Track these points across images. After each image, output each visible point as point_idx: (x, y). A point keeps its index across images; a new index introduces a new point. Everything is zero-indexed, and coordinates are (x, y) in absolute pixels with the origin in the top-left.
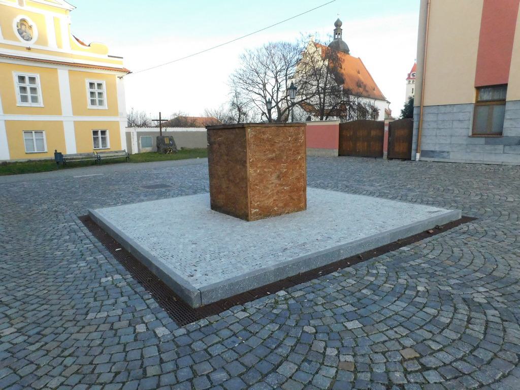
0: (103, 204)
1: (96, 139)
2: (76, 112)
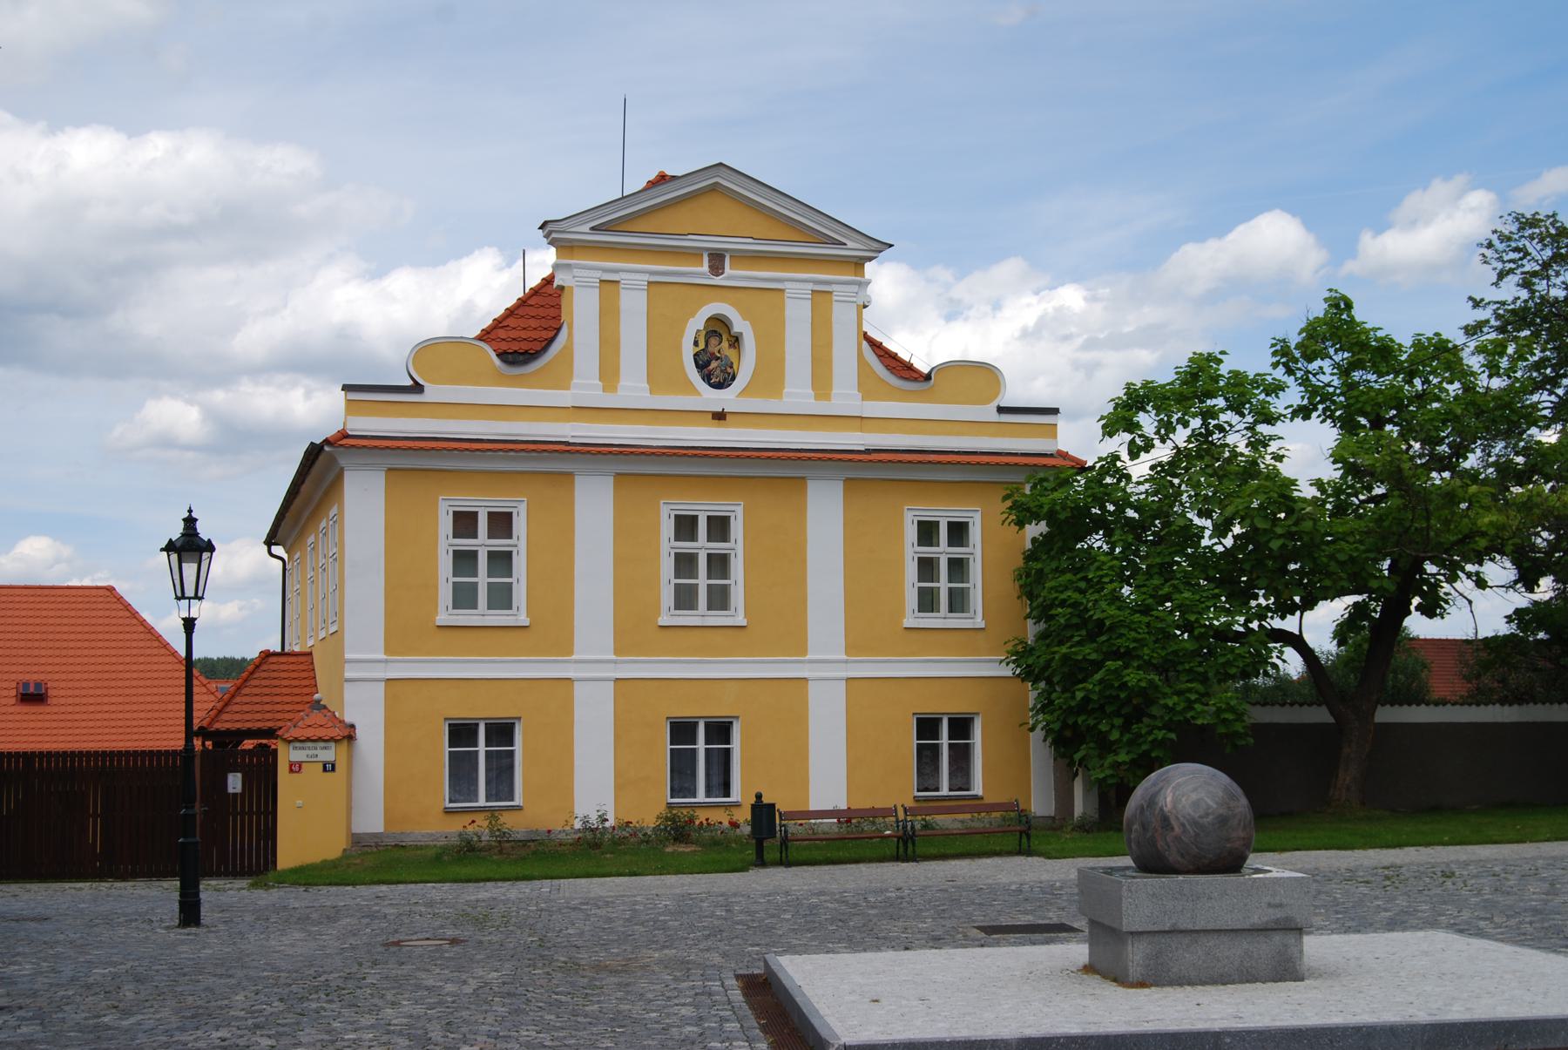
0: (791, 950)
1: (927, 758)
2: (857, 644)
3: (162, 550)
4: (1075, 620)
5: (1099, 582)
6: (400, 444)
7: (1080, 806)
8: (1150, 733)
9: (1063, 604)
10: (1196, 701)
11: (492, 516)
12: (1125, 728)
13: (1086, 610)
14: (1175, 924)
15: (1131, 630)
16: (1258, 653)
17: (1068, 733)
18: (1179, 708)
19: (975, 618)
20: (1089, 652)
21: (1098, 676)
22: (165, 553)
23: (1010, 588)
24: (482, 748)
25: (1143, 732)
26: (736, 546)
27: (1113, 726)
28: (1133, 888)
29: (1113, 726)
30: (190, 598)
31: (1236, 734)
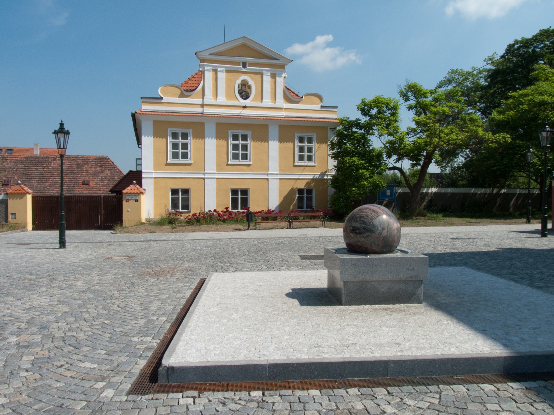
3: (53, 133)
6: (156, 113)
22: (54, 134)
24: (180, 196)
28: (345, 262)
30: (62, 149)
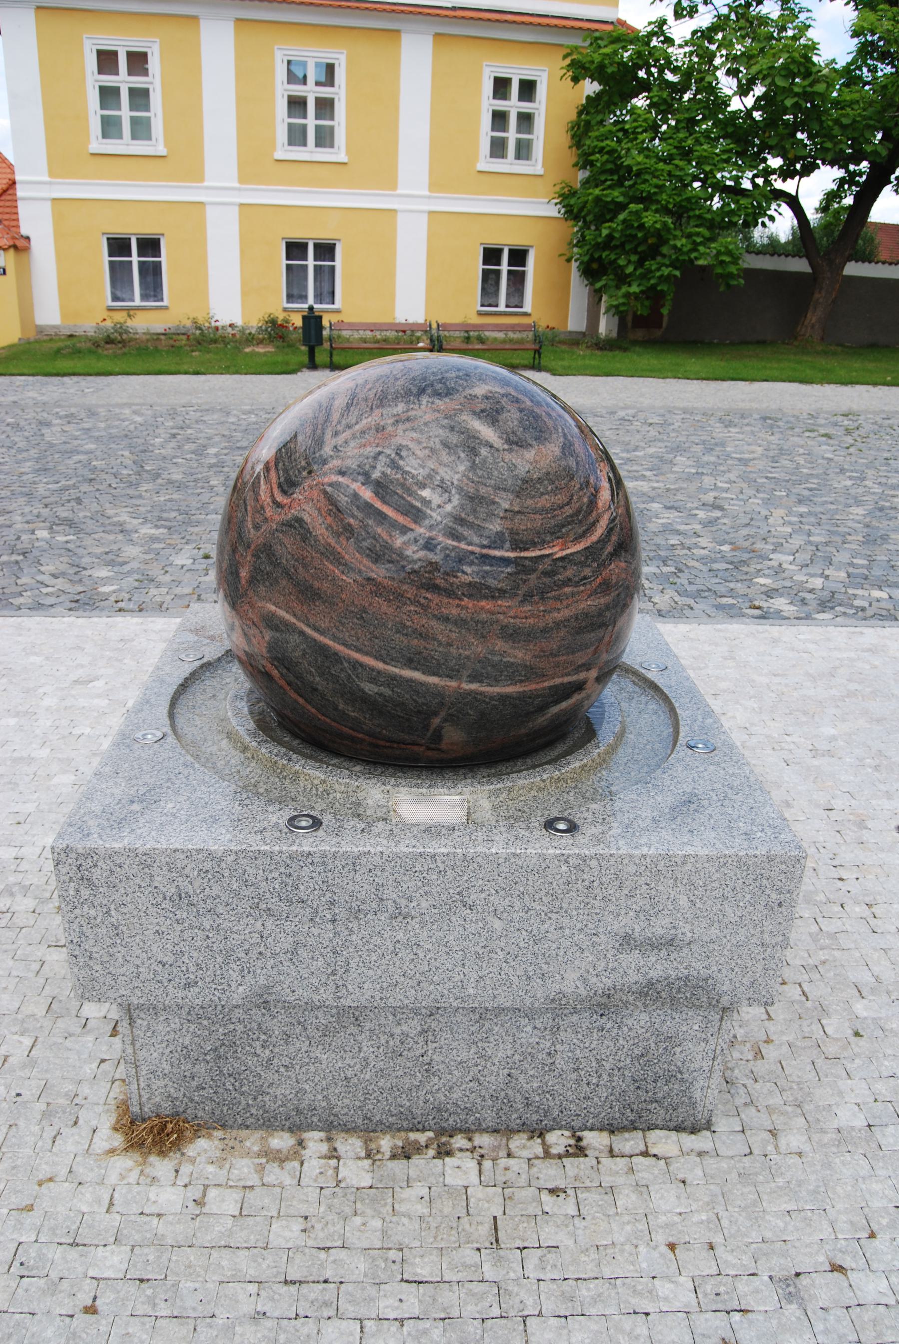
1: (490, 280)
2: (438, 184)
4: (610, 166)
5: (633, 133)
7: (605, 327)
8: (658, 270)
9: (601, 151)
10: (701, 244)
11: (131, 55)
12: (640, 263)
13: (620, 157)
14: (268, 988)
15: (655, 177)
16: (760, 206)
17: (595, 266)
18: (685, 249)
19: (536, 166)
20: (616, 195)
21: (621, 217)
23: (564, 139)
25: (653, 268)
26: (339, 93)
27: (629, 262)
29: (629, 262)
31: (731, 276)
